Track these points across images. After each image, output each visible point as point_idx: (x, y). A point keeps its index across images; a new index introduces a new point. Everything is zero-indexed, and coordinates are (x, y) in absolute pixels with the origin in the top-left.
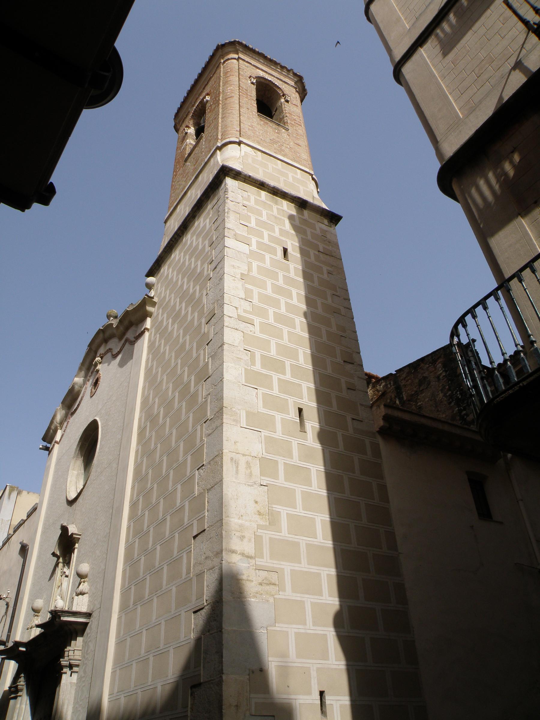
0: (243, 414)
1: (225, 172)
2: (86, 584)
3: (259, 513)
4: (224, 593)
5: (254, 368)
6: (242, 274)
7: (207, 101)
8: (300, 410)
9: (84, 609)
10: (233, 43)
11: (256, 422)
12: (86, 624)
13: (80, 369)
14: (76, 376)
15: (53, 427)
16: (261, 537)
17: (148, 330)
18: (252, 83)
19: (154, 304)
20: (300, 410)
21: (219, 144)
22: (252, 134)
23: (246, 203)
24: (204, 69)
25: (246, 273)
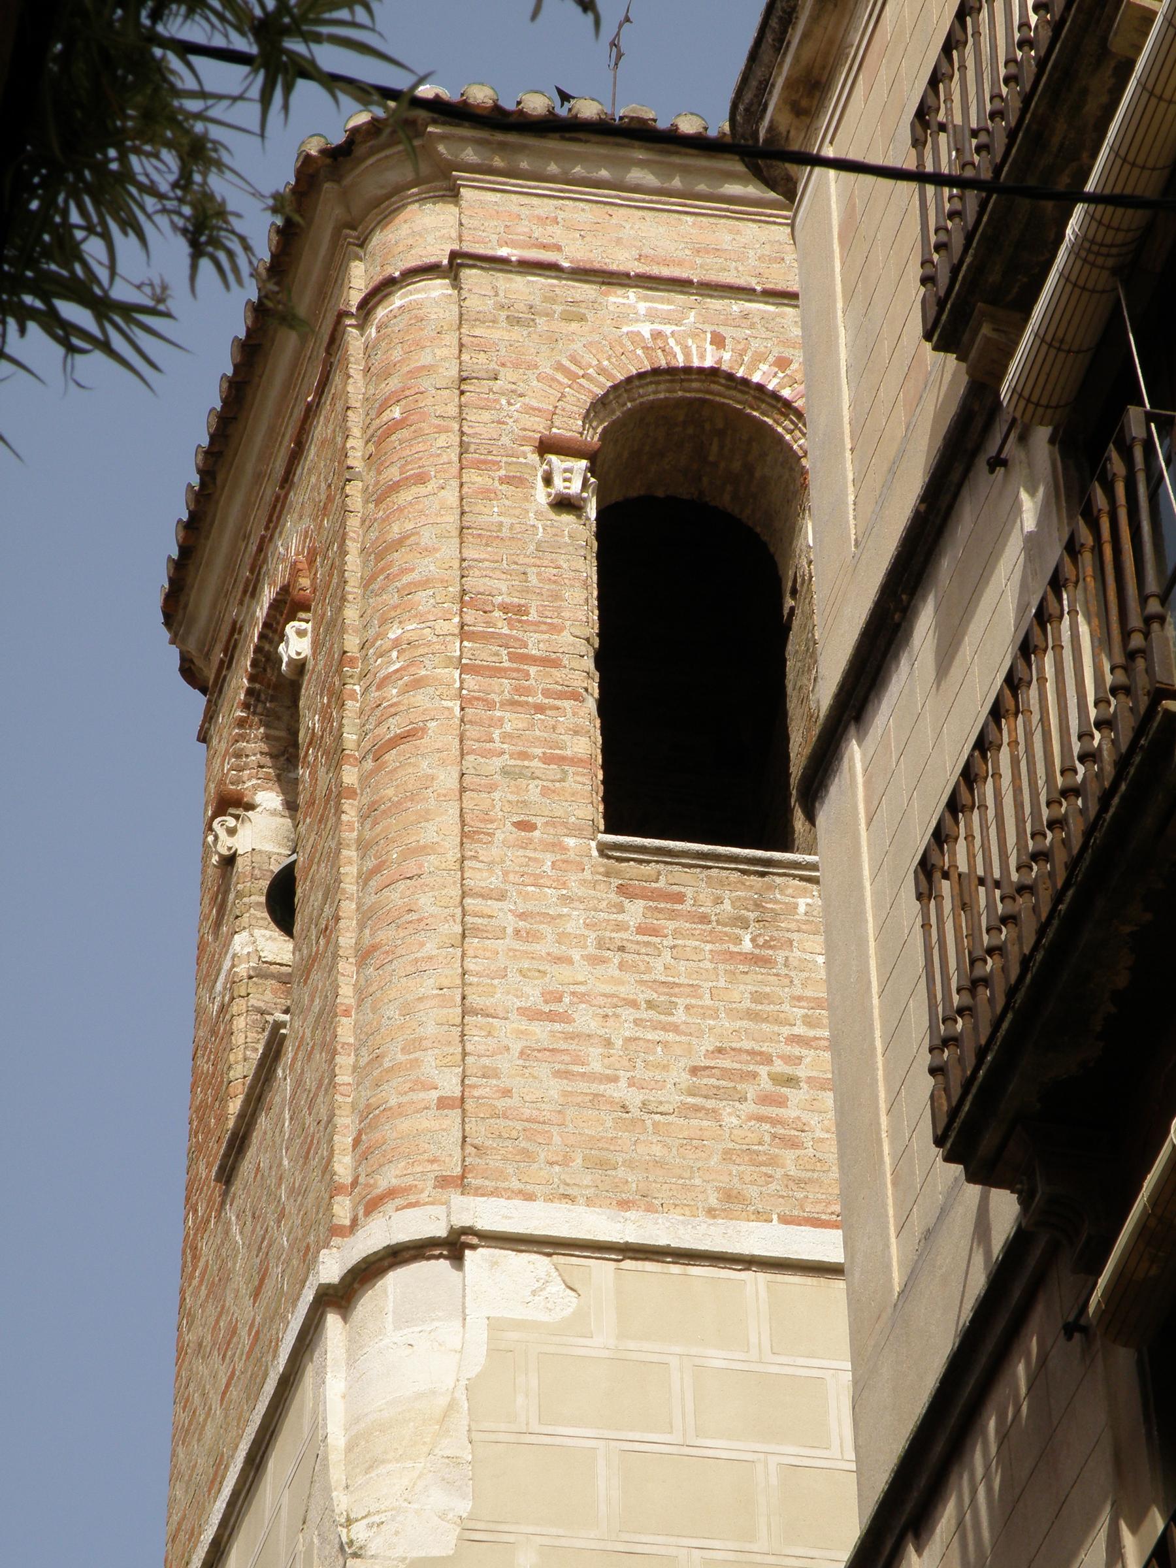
7: (300, 667)
18: (565, 504)
21: (331, 1268)
22: (555, 1088)
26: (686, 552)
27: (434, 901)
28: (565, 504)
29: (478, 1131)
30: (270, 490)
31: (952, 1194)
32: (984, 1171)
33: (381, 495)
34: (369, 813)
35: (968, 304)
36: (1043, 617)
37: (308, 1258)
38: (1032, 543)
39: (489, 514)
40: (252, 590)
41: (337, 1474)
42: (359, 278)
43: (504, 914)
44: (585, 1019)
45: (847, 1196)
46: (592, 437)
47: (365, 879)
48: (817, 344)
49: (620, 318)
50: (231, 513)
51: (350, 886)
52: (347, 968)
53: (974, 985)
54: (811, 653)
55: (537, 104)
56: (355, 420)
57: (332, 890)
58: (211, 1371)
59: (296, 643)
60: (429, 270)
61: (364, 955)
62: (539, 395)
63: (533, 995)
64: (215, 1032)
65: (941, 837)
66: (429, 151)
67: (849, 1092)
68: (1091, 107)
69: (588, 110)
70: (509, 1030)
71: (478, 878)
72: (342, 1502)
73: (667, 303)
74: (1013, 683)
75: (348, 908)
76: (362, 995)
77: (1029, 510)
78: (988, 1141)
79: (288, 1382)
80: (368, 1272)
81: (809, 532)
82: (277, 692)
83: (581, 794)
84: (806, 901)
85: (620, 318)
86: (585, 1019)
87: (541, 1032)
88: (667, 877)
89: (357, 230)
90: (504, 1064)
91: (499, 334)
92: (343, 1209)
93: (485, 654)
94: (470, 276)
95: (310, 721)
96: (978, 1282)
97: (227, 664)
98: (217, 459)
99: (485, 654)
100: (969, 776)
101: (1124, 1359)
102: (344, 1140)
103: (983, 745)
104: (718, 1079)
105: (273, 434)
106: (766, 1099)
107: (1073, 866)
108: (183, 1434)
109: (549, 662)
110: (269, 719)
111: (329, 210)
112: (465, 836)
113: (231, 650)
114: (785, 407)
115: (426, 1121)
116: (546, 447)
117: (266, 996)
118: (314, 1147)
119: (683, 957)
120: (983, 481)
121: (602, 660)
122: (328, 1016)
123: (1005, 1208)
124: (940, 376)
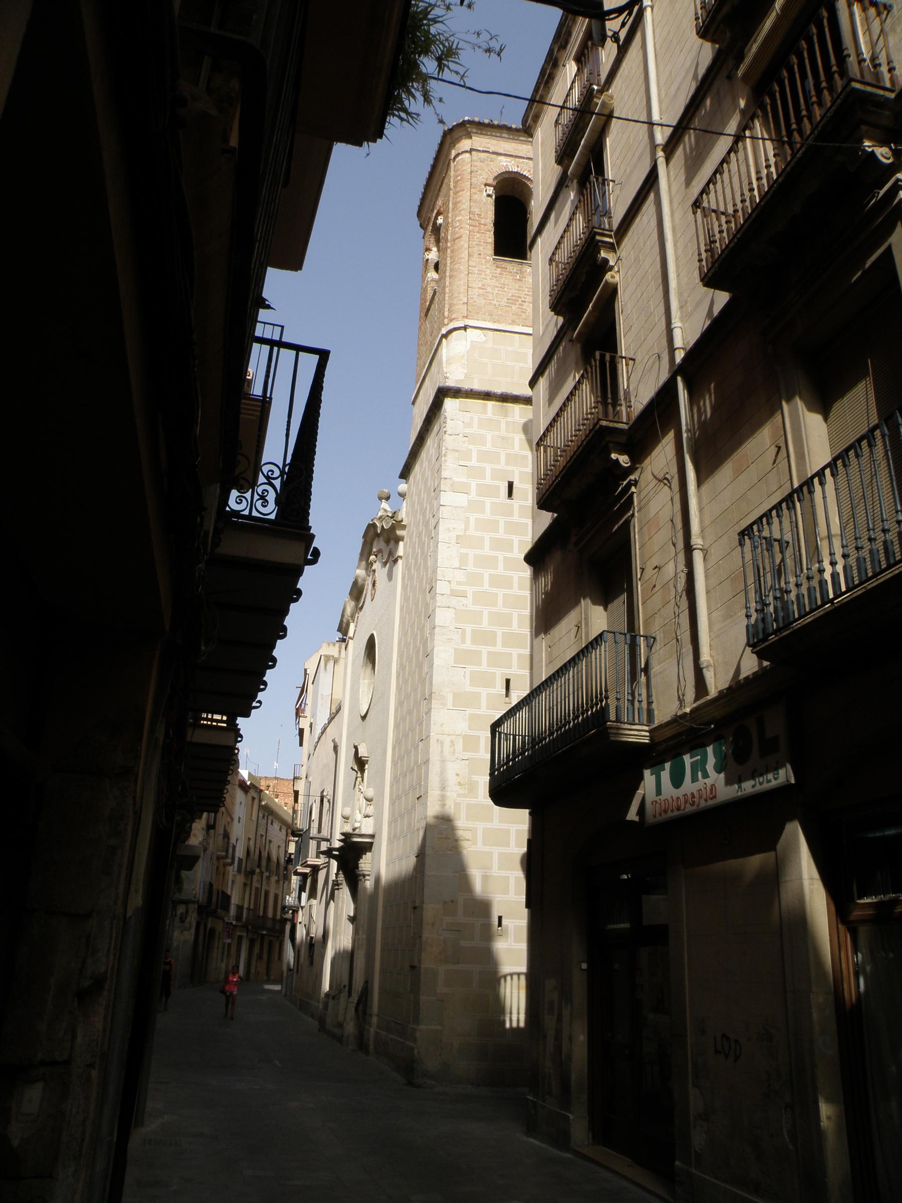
0: (450, 698)
1: (443, 393)
2: (372, 807)
3: (460, 784)
4: (427, 848)
5: (463, 647)
6: (458, 536)
7: (441, 225)
8: (508, 682)
9: (370, 831)
10: (463, 124)
11: (463, 700)
12: (372, 843)
13: (361, 560)
14: (358, 568)
15: (345, 620)
16: (460, 804)
17: (401, 557)
18: (489, 196)
19: (404, 527)
20: (508, 682)
21: (444, 331)
22: (483, 302)
23: (467, 431)
24: (434, 167)
25: (462, 534)
26: (510, 199)
27: (463, 267)
28: (489, 196)
29: (470, 309)
30: (436, 192)
31: (552, 317)
32: (557, 313)
33: (456, 193)
34: (452, 251)
35: (564, 156)
36: (574, 214)
37: (440, 329)
38: (572, 201)
39: (476, 197)
40: (433, 211)
41: (444, 365)
42: (453, 153)
43: (476, 270)
44: (489, 289)
45: (533, 320)
46: (494, 183)
47: (451, 263)
48: (535, 167)
49: (500, 161)
50: (430, 196)
51: (448, 264)
52: (448, 279)
53: (558, 280)
54: (532, 225)
55: (487, 121)
56: (452, 180)
57: (445, 265)
58: (423, 348)
59: (440, 220)
60: (466, 152)
61: (451, 277)
62: (485, 175)
63: (480, 285)
64: (424, 290)
65: (554, 254)
66: (467, 130)
67: (535, 303)
68: (587, 120)
69: (496, 123)
70: (475, 291)
71: (471, 263)
72: (445, 370)
73: (509, 159)
74: (568, 226)
75: (448, 268)
76: (450, 283)
77: (572, 195)
78: (558, 308)
79: (436, 350)
80: (450, 332)
81: (533, 203)
82: (437, 230)
83: (490, 249)
84: (529, 270)
85: (500, 161)
86: (489, 289)
87: (481, 291)
88: (504, 265)
89: (453, 144)
90: (475, 297)
91: (478, 164)
92: (446, 321)
93: (474, 223)
94: (473, 153)
95: (442, 235)
96: (555, 333)
97: (428, 225)
98: (427, 186)
99: (474, 223)
100: (559, 243)
101: (579, 346)
102: (446, 309)
103: (562, 237)
104: (512, 301)
105: (437, 182)
106: (520, 305)
107: (577, 259)
108: (419, 359)
109: (485, 225)
110: (435, 235)
111: (448, 140)
112: (469, 256)
113: (429, 222)
114: (529, 179)
115: (461, 306)
116: (486, 185)
117: (433, 284)
118: (441, 311)
119: (507, 279)
120: (564, 190)
121: (495, 224)
122: (444, 287)
123: (561, 320)
124: (558, 169)
